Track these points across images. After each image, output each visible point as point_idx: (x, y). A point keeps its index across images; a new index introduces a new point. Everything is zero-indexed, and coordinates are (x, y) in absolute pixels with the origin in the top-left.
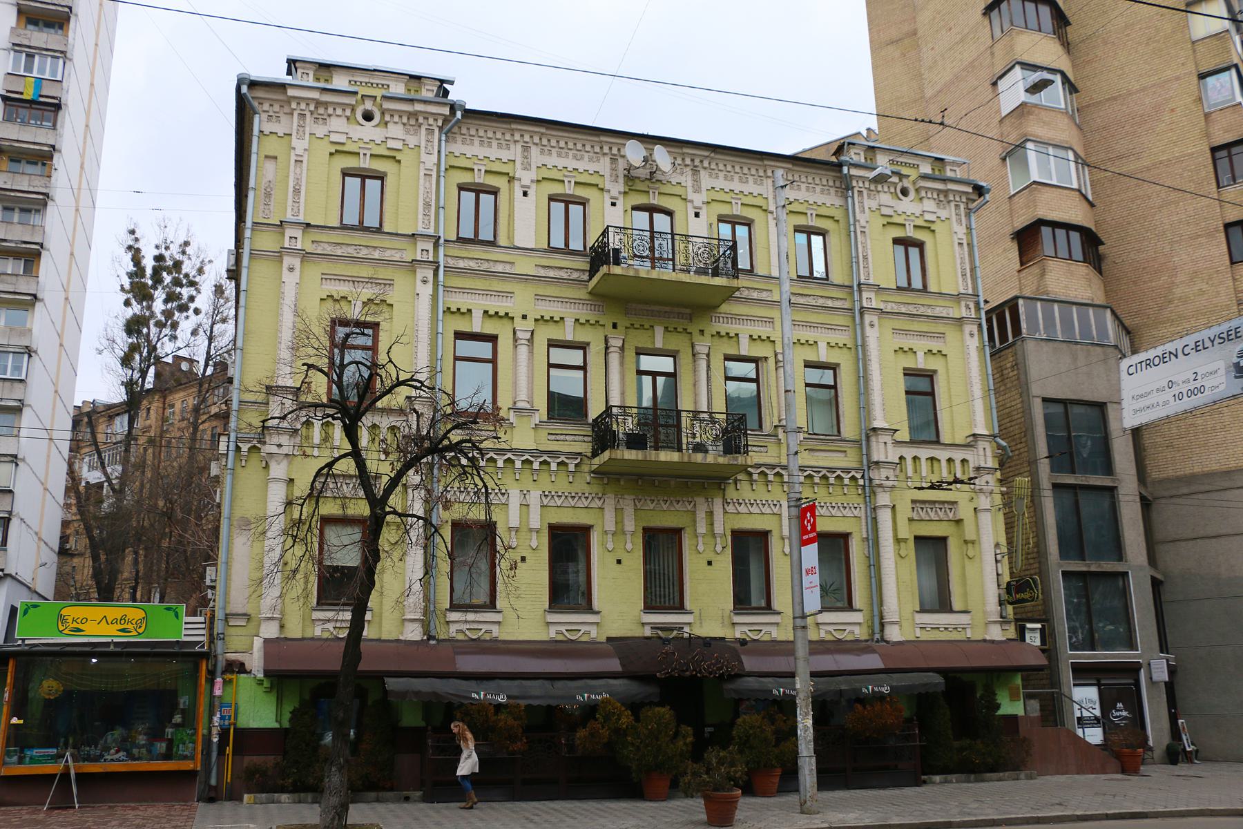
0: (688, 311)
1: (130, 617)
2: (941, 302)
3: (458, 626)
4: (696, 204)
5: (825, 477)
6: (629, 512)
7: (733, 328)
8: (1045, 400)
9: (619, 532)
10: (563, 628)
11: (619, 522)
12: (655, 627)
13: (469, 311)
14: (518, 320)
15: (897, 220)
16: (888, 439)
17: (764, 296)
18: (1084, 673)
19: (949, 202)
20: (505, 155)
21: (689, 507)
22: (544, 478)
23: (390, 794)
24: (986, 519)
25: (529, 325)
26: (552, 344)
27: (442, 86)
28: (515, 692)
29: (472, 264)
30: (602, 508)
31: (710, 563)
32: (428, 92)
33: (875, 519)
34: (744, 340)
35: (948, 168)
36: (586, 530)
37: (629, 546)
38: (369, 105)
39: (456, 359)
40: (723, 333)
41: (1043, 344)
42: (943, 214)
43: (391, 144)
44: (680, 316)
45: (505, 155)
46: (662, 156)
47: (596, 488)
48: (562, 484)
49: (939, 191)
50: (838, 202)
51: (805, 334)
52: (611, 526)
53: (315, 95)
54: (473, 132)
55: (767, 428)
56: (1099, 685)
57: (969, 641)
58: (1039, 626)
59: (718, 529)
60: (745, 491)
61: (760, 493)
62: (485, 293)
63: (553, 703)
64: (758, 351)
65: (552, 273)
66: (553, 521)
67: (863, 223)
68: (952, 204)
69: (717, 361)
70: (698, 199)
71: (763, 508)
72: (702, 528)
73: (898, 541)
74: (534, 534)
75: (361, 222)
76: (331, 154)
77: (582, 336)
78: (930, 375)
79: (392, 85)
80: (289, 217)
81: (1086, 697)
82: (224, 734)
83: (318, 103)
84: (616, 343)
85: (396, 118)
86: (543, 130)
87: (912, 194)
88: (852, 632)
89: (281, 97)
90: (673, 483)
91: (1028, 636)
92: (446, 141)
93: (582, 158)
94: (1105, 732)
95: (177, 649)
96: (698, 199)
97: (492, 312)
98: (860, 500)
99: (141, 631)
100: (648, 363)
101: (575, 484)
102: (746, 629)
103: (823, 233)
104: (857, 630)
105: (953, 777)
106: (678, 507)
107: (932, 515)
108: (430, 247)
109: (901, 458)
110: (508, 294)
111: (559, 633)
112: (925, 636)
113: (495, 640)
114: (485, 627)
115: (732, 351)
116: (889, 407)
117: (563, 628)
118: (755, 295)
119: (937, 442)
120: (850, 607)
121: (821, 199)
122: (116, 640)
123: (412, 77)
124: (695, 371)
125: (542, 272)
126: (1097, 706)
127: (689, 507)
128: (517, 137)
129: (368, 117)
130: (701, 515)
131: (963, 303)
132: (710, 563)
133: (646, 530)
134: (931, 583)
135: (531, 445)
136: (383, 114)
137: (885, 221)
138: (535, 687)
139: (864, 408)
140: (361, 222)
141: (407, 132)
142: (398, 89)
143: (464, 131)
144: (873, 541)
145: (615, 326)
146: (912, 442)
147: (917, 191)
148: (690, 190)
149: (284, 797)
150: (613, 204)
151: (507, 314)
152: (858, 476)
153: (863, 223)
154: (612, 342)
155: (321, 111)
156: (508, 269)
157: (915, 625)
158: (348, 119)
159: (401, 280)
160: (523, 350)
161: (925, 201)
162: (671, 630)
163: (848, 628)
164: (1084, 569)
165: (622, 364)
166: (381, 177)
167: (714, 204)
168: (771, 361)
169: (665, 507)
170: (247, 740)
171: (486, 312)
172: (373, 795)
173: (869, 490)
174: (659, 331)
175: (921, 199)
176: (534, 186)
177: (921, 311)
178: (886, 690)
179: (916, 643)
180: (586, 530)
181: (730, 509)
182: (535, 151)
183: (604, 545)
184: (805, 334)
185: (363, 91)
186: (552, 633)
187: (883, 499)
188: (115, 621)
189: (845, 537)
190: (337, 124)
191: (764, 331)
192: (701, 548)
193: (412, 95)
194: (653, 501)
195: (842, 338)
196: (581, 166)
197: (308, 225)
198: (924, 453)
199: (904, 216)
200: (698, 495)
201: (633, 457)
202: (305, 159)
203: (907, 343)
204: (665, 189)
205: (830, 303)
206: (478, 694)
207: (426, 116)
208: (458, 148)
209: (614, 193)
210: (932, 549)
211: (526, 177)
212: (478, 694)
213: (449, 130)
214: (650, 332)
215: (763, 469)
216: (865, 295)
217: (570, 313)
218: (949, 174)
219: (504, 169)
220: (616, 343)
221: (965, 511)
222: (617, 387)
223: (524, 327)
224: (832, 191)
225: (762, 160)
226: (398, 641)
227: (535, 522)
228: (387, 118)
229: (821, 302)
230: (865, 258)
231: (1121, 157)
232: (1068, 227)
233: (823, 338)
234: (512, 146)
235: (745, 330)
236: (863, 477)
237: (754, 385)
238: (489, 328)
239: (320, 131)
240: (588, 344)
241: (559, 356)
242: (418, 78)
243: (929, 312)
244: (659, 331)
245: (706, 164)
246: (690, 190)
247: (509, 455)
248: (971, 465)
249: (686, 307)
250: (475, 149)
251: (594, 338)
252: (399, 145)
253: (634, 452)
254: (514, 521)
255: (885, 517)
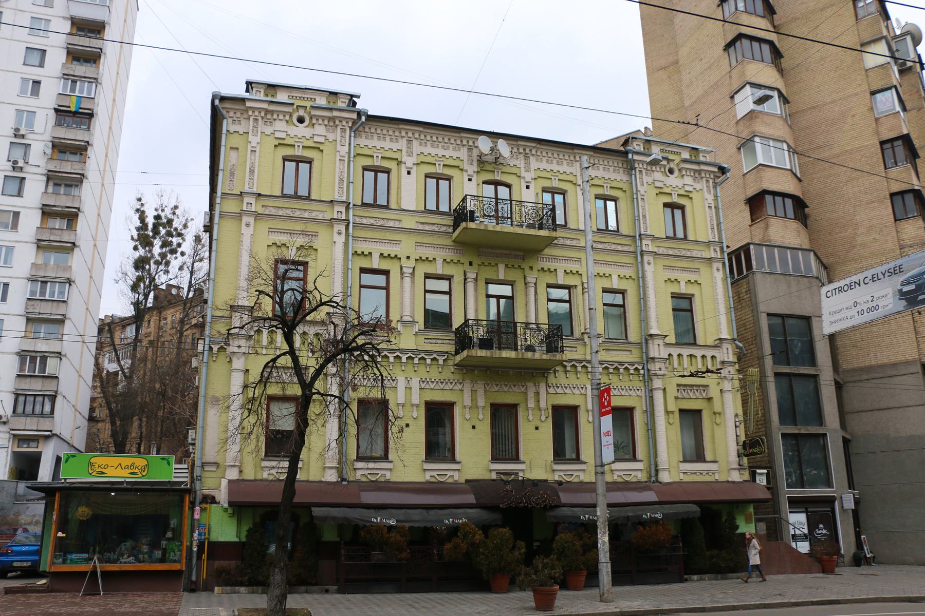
0: (521, 253)
1: (137, 464)
2: (696, 247)
3: (362, 471)
4: (527, 179)
5: (616, 369)
6: (481, 392)
7: (552, 265)
8: (769, 315)
9: (474, 407)
10: (435, 474)
11: (474, 400)
12: (499, 472)
13: (370, 253)
14: (404, 260)
15: (289, 141)
16: (661, 342)
17: (574, 243)
18: (796, 504)
19: (702, 178)
20: (395, 146)
21: (523, 390)
22: (422, 371)
23: (315, 588)
24: (728, 397)
25: (412, 263)
26: (428, 276)
27: (352, 99)
28: (402, 518)
29: (372, 221)
30: (462, 390)
31: (537, 428)
32: (342, 103)
33: (652, 398)
34: (560, 274)
35: (701, 155)
36: (451, 405)
37: (481, 417)
38: (301, 112)
39: (361, 286)
40: (546, 269)
41: (767, 276)
42: (331, 137)
43: (316, 139)
44: (516, 257)
45: (395, 146)
46: (504, 148)
47: (458, 377)
48: (434, 373)
49: (695, 171)
50: (625, 178)
51: (603, 270)
52: (468, 402)
53: (265, 106)
54: (373, 130)
55: (577, 334)
56: (807, 512)
57: (717, 482)
58: (765, 471)
59: (543, 404)
60: (561, 378)
61: (572, 379)
62: (382, 241)
63: (428, 525)
64: (570, 281)
65: (427, 228)
66: (428, 399)
67: (642, 192)
68: (704, 180)
69: (542, 288)
70: (528, 176)
71: (574, 390)
72: (531, 404)
73: (668, 413)
74: (415, 408)
75: (296, 192)
76: (276, 146)
77: (448, 271)
78: (689, 298)
79: (318, 99)
80: (247, 189)
81: (797, 520)
82: (201, 545)
83: (267, 112)
84: (471, 275)
85: (320, 121)
86: (421, 129)
87: (676, 173)
88: (452, 477)
89: (242, 107)
90: (511, 372)
91: (758, 478)
92: (355, 137)
93: (448, 148)
94: (811, 545)
95: (169, 487)
96: (528, 176)
97: (385, 255)
98: (641, 384)
99: (144, 474)
100: (494, 289)
101: (443, 374)
102: (562, 474)
103: (615, 200)
104: (639, 474)
105: (706, 576)
106: (515, 389)
107: (691, 395)
108: (343, 209)
109: (670, 355)
110: (396, 242)
111: (432, 476)
112: (686, 479)
113: (388, 482)
114: (381, 473)
115: (553, 281)
116: (661, 320)
117: (435, 474)
118: (568, 242)
119: (694, 344)
120: (634, 459)
121: (613, 176)
122: (127, 480)
123: (331, 93)
124: (526, 295)
125: (421, 227)
126: (806, 527)
127: (523, 390)
128: (403, 134)
129: (301, 120)
130: (531, 395)
131: (712, 248)
132: (537, 428)
133: (492, 405)
134: (691, 442)
135: (412, 346)
136: (311, 118)
137: (658, 191)
138: (416, 514)
139: (644, 320)
140: (296, 192)
141: (328, 131)
142: (322, 101)
143: (367, 130)
144: (650, 412)
145: (471, 264)
146: (678, 344)
147: (680, 170)
148: (523, 170)
149: (242, 589)
150: (470, 180)
151: (396, 256)
152: (640, 368)
153: (642, 192)
154: (469, 275)
155: (269, 116)
156: (397, 224)
157: (679, 471)
158: (287, 122)
159: (323, 232)
160: (407, 281)
161: (685, 177)
162: (510, 474)
163: (633, 473)
164: (797, 432)
165: (476, 290)
166: (310, 162)
167: (539, 180)
168: (580, 288)
169: (506, 389)
170: (217, 549)
171: (382, 254)
172: (303, 588)
173: (648, 377)
174: (501, 267)
175: (683, 176)
176: (415, 167)
177: (683, 253)
178: (659, 516)
179: (681, 483)
180: (451, 405)
181: (551, 390)
182: (415, 143)
183: (463, 416)
184: (606, 270)
185: (297, 103)
186: (427, 477)
187: (657, 383)
188: (127, 467)
189: (631, 410)
190: (280, 125)
191: (574, 267)
192: (531, 418)
193: (331, 106)
194: (497, 385)
195: (629, 272)
196: (447, 153)
197: (260, 195)
198: (686, 351)
199: (671, 188)
200: (529, 381)
201: (508, 356)
202: (258, 150)
203: (673, 275)
204: (505, 169)
205: (620, 248)
206: (376, 519)
207: (341, 119)
208: (362, 141)
209: (470, 172)
210: (691, 419)
211: (410, 161)
212: (376, 519)
213: (357, 130)
214: (495, 268)
215: (584, 363)
216: (644, 242)
217: (440, 255)
218: (702, 159)
219: (394, 156)
220: (471, 275)
221: (714, 392)
222: (472, 306)
223: (408, 265)
224: (621, 170)
225: (573, 149)
226: (321, 482)
227: (416, 399)
228: (314, 121)
229: (613, 247)
230: (644, 217)
231: (819, 147)
232: (784, 195)
233: (615, 272)
234: (400, 140)
235: (561, 267)
236: (643, 368)
237: (567, 305)
238: (384, 266)
239: (268, 130)
240: (452, 276)
241: (432, 285)
242: (335, 94)
243: (689, 254)
244: (501, 267)
245: (534, 152)
246: (523, 170)
247: (398, 353)
248: (718, 360)
249: (520, 250)
250: (375, 142)
251: (456, 272)
252: (322, 140)
253: (484, 351)
254: (401, 400)
255: (658, 396)
